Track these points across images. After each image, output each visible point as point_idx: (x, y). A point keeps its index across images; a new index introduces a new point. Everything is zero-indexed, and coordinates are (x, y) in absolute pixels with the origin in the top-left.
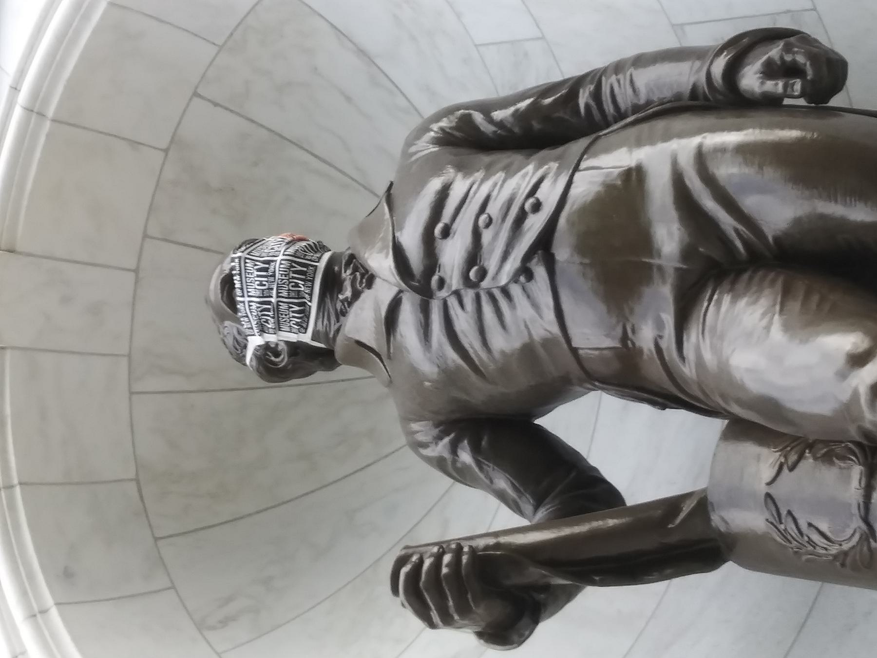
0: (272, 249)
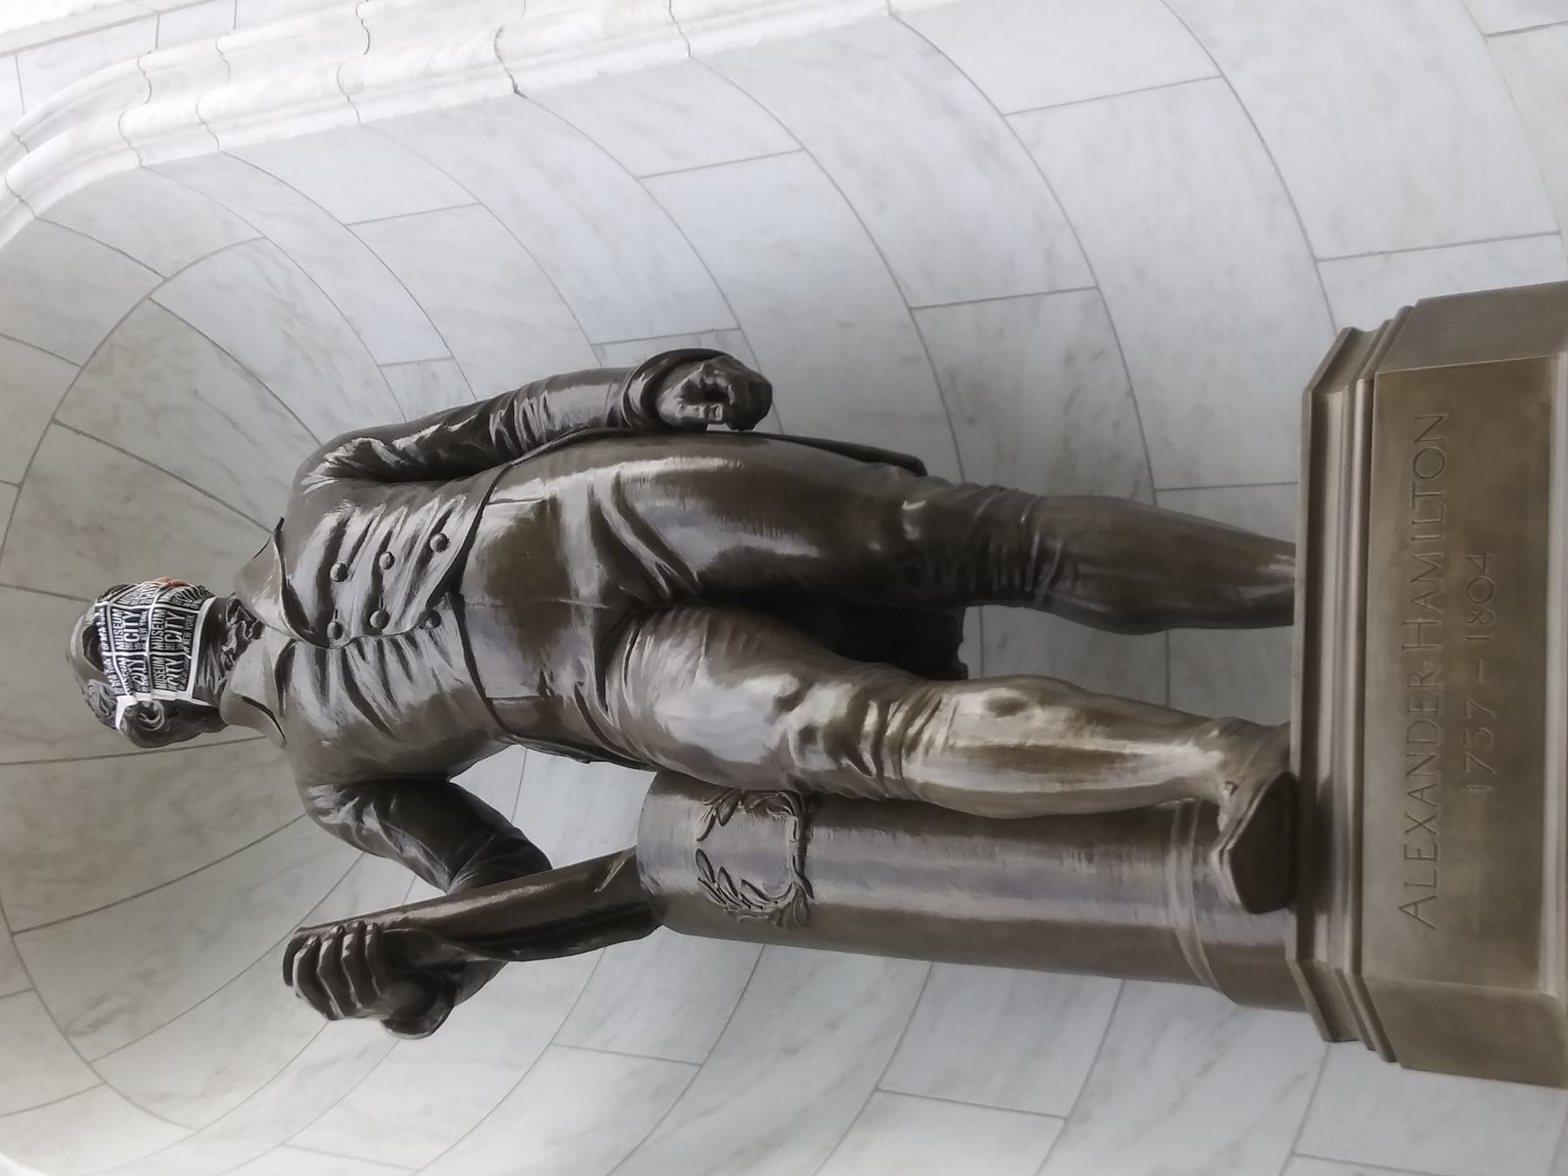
0: (144, 596)
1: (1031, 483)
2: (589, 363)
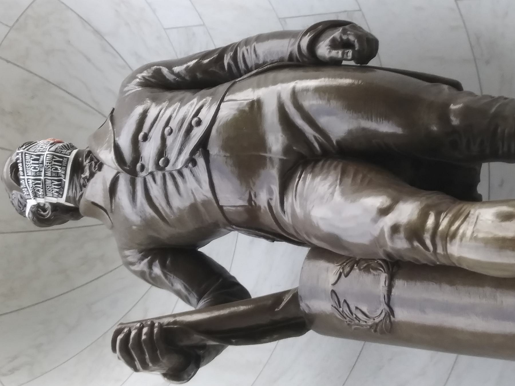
2: (277, 28)
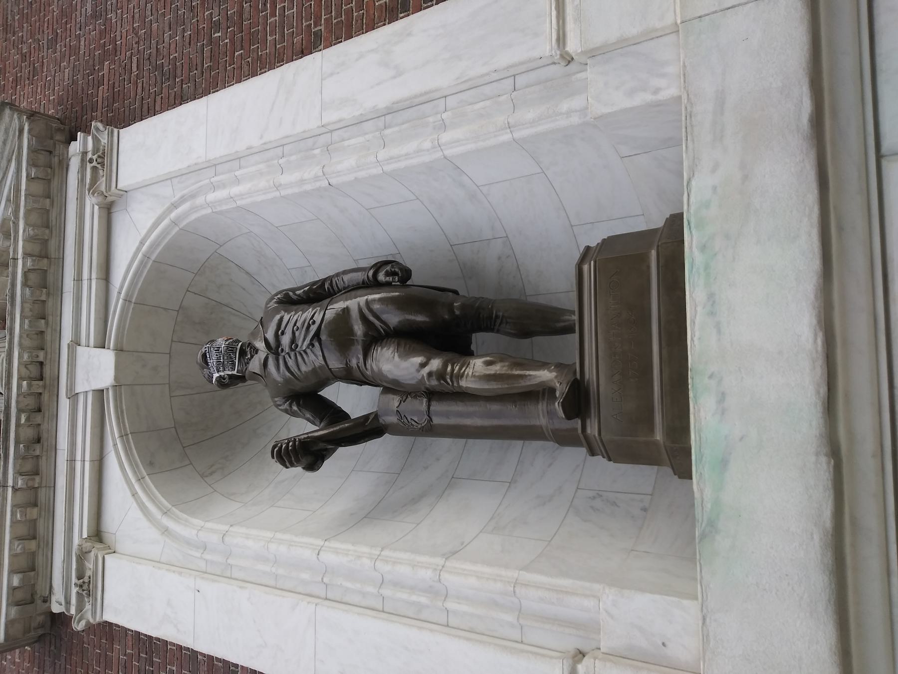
1: (490, 295)
2: (354, 266)
